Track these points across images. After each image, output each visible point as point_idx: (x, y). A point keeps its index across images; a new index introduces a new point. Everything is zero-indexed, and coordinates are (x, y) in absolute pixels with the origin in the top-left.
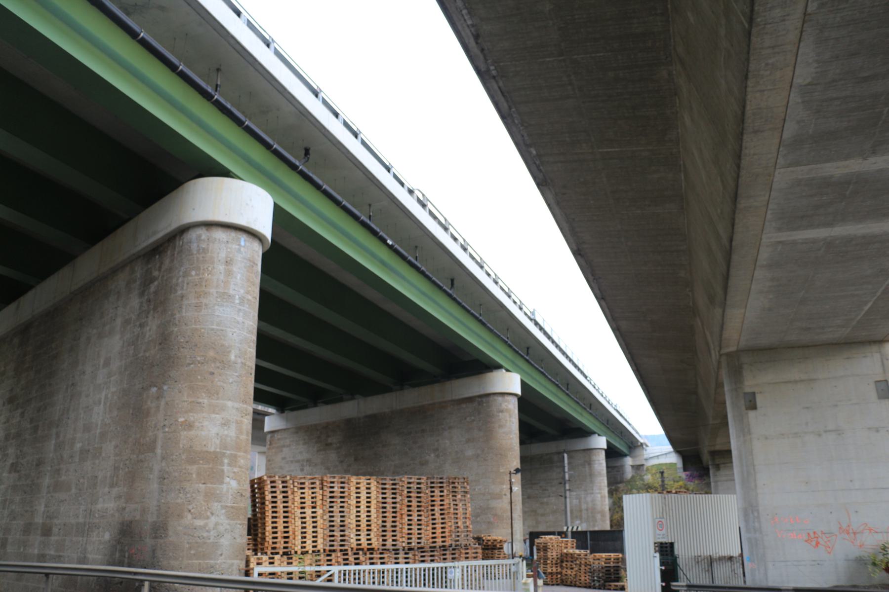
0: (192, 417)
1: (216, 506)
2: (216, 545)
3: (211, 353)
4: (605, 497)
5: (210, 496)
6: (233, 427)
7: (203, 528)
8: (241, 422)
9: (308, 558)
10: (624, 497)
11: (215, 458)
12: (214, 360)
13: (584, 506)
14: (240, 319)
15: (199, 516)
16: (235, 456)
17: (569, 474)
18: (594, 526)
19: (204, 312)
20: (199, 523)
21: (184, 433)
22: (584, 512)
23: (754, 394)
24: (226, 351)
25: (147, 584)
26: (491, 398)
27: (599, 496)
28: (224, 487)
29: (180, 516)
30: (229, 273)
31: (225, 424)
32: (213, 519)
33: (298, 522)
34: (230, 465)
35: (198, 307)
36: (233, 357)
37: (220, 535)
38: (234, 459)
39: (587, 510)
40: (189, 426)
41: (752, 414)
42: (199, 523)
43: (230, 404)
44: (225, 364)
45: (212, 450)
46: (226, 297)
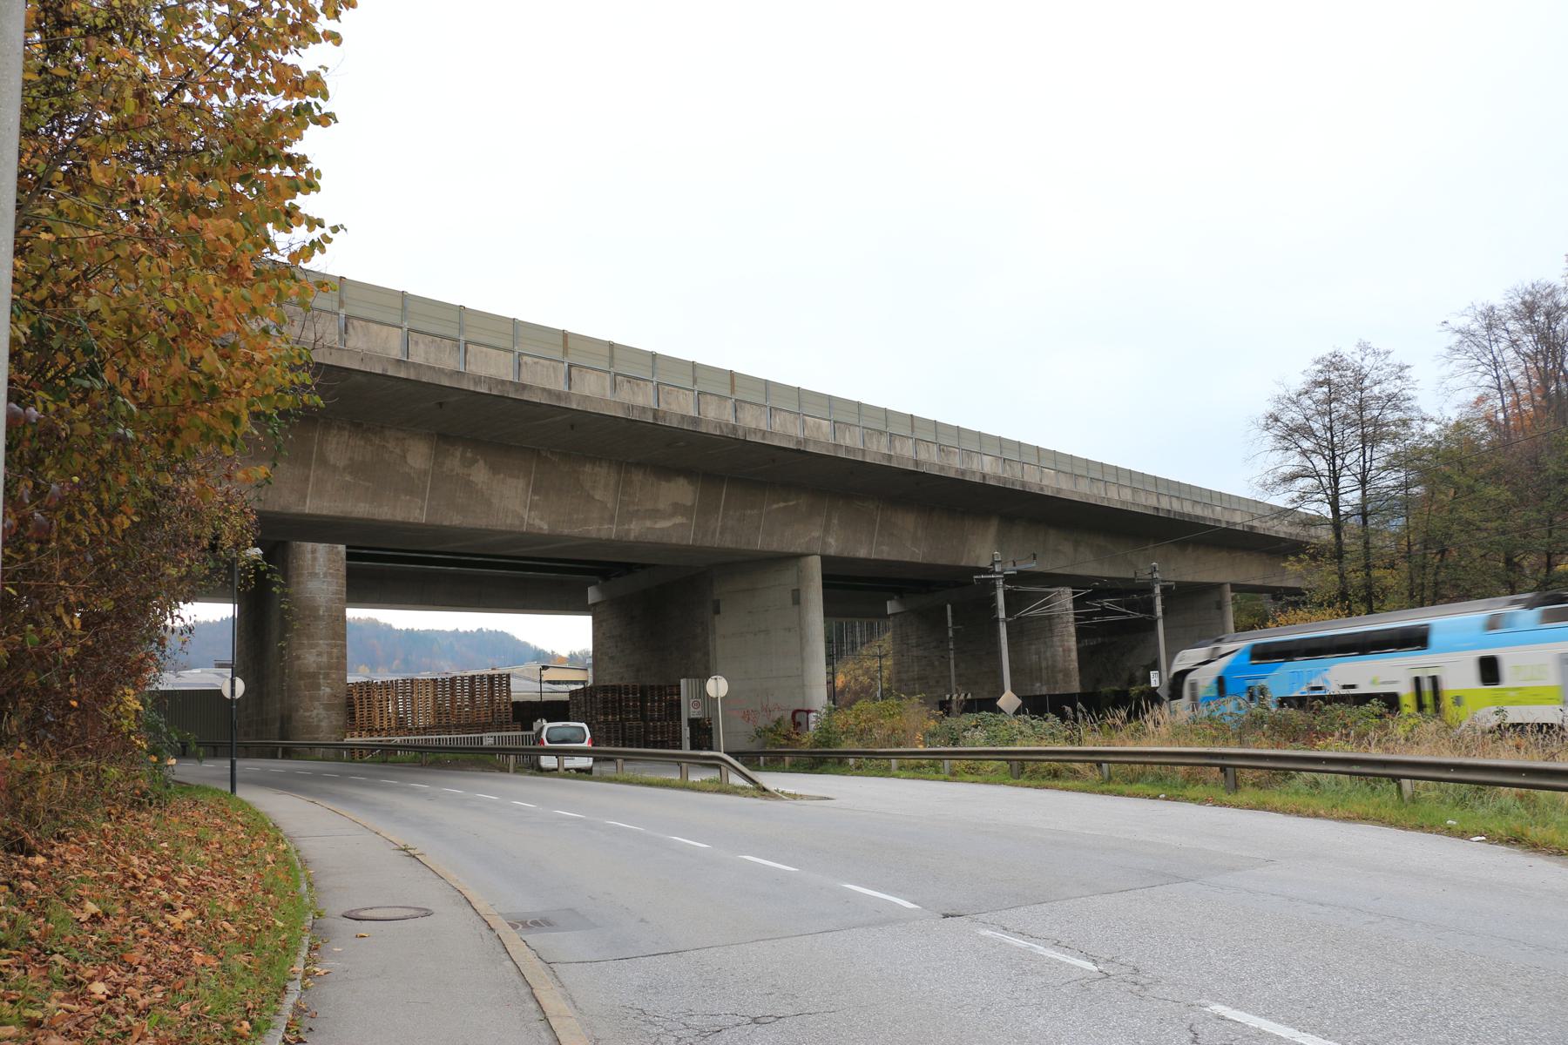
0: (299, 652)
1: (317, 703)
2: (318, 727)
3: (307, 613)
4: (1070, 650)
5: (312, 698)
6: (325, 656)
7: (310, 716)
8: (331, 653)
9: (384, 733)
10: (515, 697)
11: (314, 676)
12: (309, 616)
13: (1044, 665)
14: (325, 587)
15: (307, 710)
16: (328, 674)
17: (954, 631)
18: (1055, 689)
19: (302, 586)
20: (307, 714)
21: (296, 663)
22: (1044, 671)
23: (719, 601)
24: (316, 609)
25: (280, 749)
26: (803, 560)
27: (1061, 649)
28: (321, 693)
29: (297, 711)
30: (314, 559)
31: (320, 654)
32: (315, 712)
33: (378, 711)
34: (324, 678)
35: (298, 583)
36: (321, 613)
37: (320, 721)
38: (327, 676)
39: (1047, 668)
40: (298, 658)
41: (717, 617)
42: (307, 714)
43: (321, 642)
44: (317, 618)
45: (312, 670)
46: (314, 575)
